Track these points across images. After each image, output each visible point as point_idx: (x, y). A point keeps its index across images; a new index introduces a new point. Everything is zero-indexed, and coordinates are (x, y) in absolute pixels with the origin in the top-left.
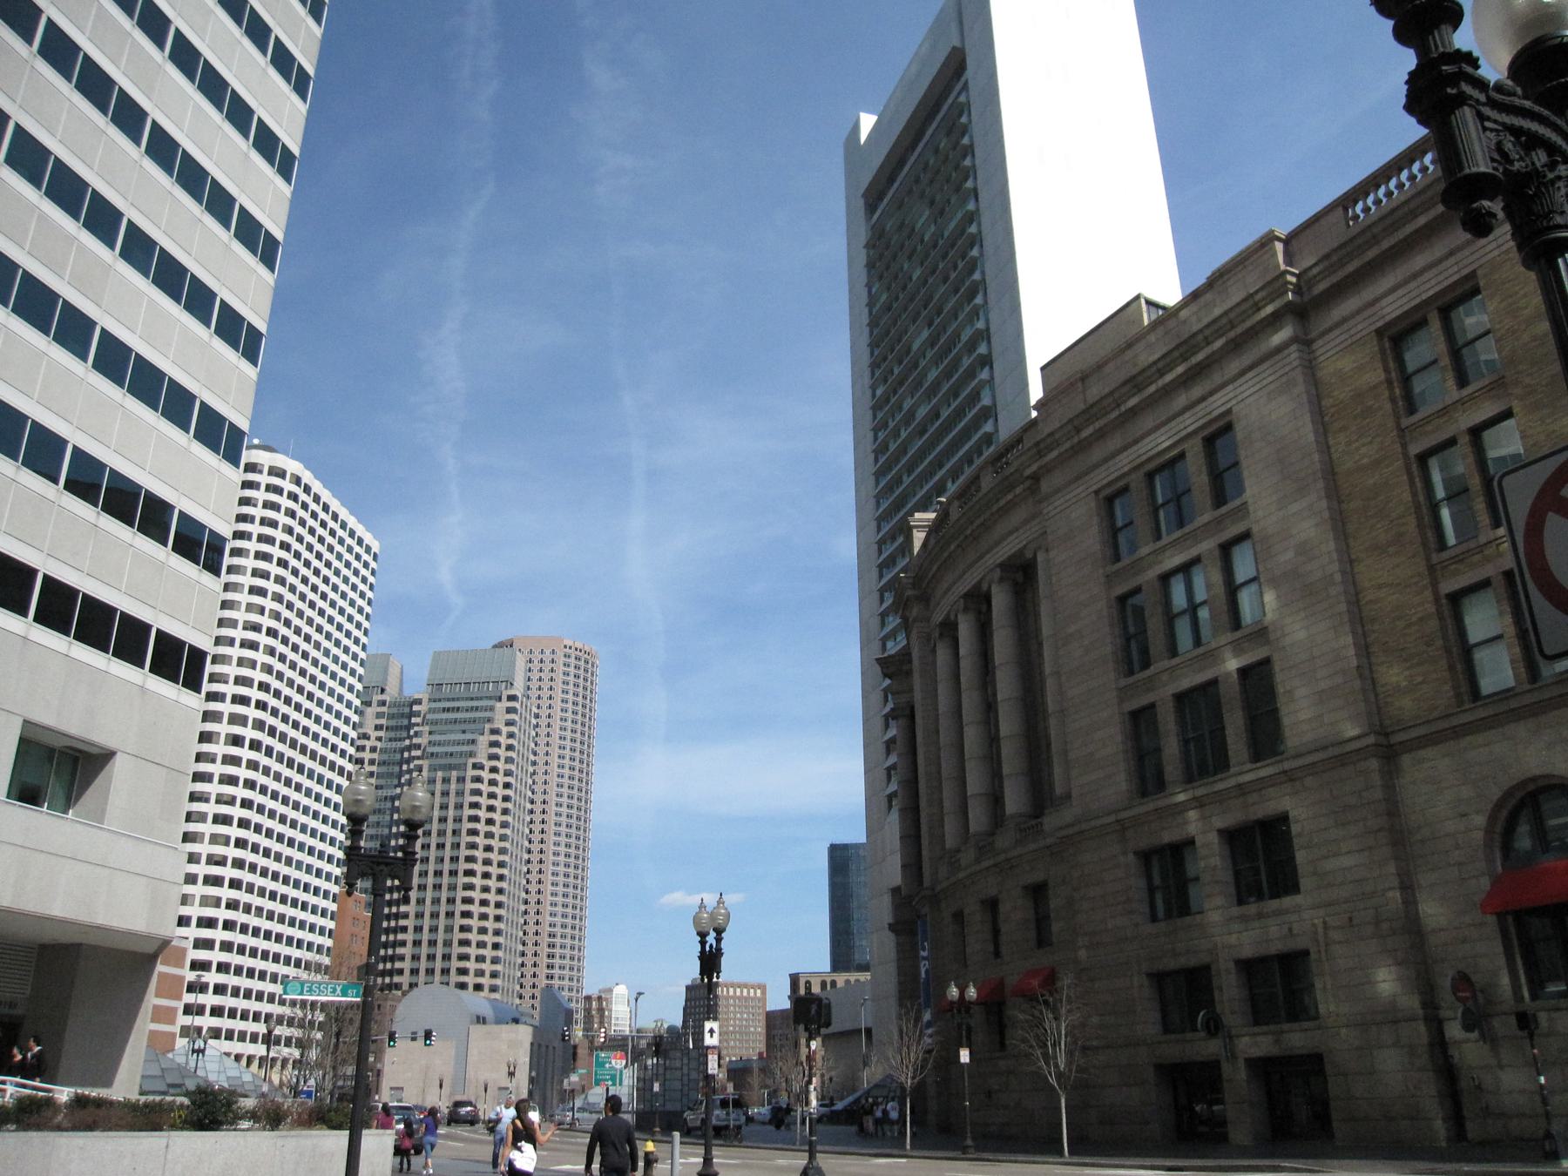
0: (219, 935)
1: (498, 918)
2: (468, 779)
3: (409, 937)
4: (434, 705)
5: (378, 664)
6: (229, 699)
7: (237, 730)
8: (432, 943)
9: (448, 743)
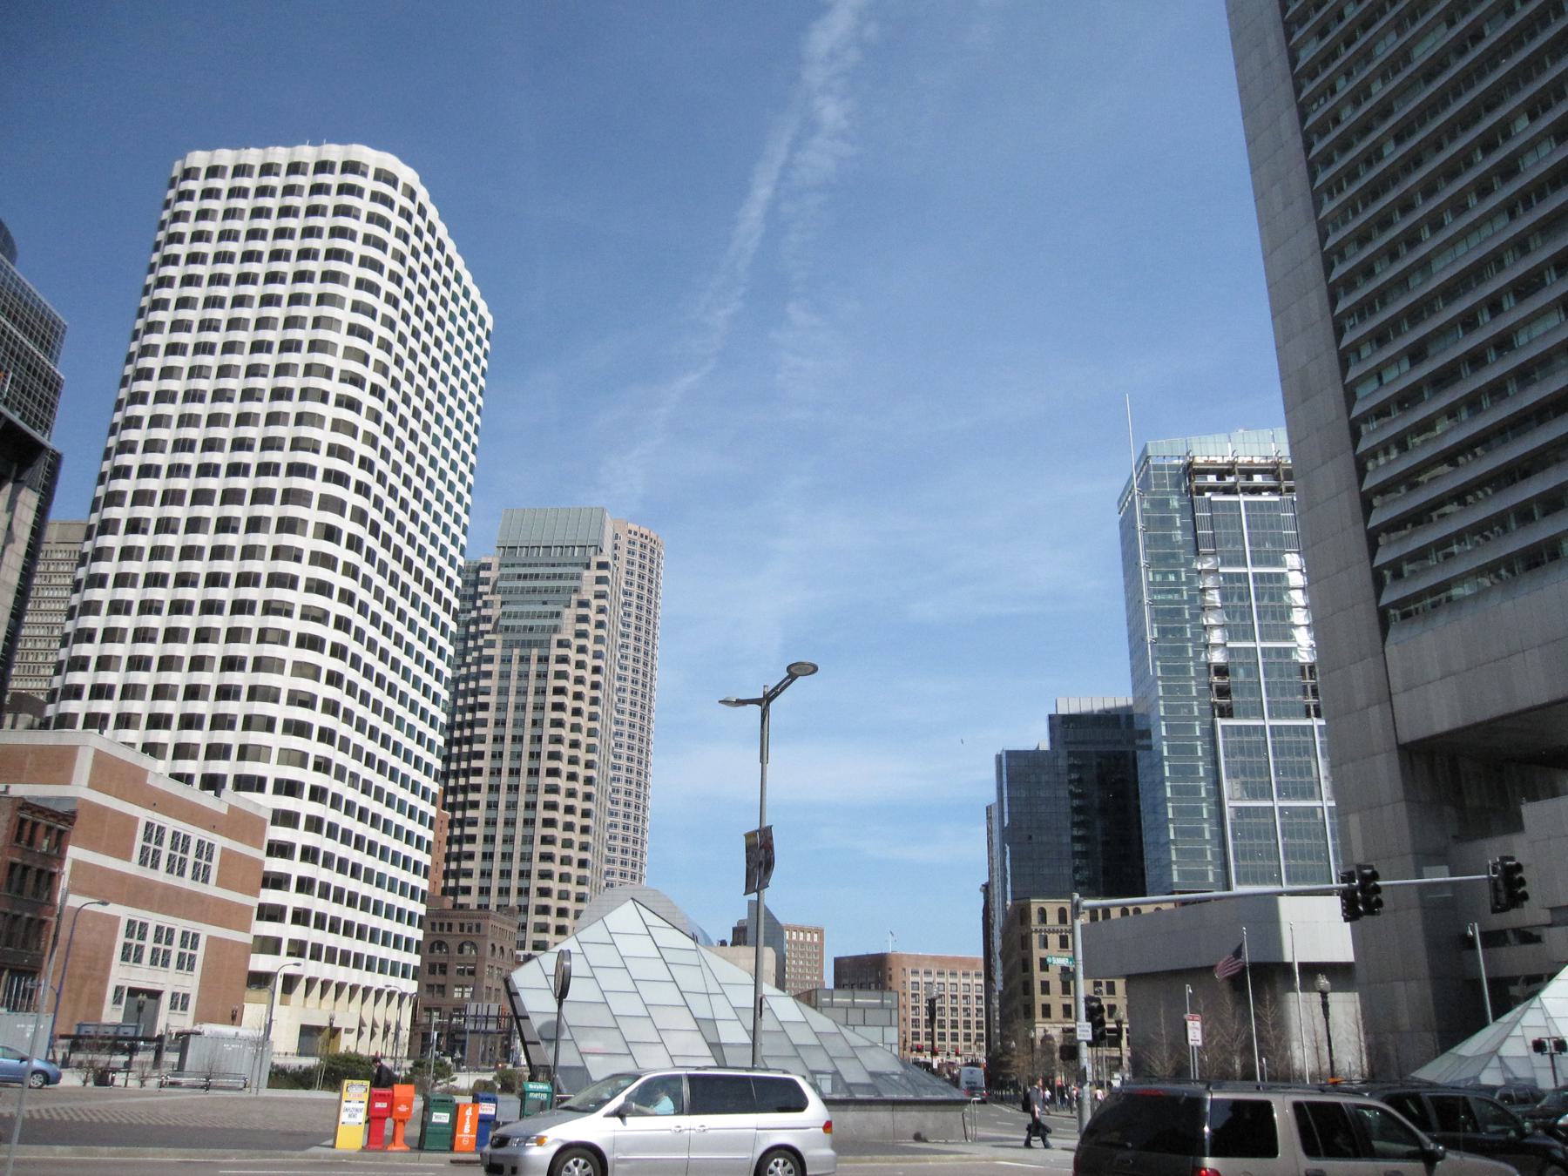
0: (304, 806)
1: (585, 830)
2: (552, 659)
3: (478, 848)
4: (505, 571)
6: (320, 474)
7: (331, 518)
8: (507, 857)
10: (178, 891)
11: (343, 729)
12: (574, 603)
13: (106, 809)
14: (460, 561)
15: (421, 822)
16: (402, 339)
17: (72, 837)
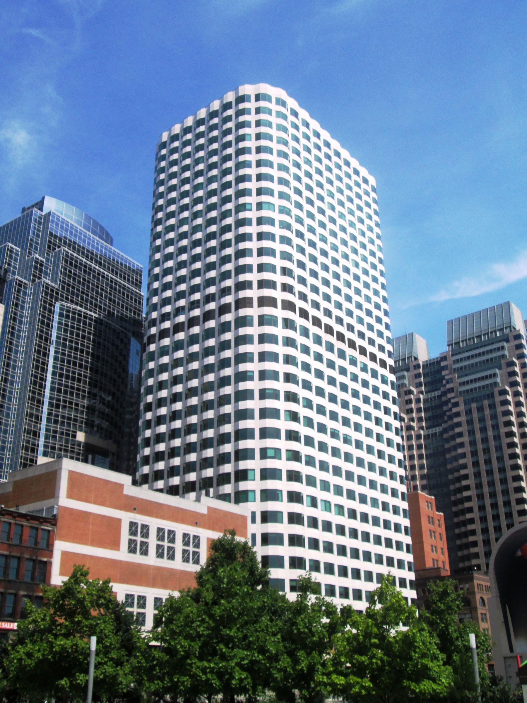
5: (407, 340)
13: (95, 503)
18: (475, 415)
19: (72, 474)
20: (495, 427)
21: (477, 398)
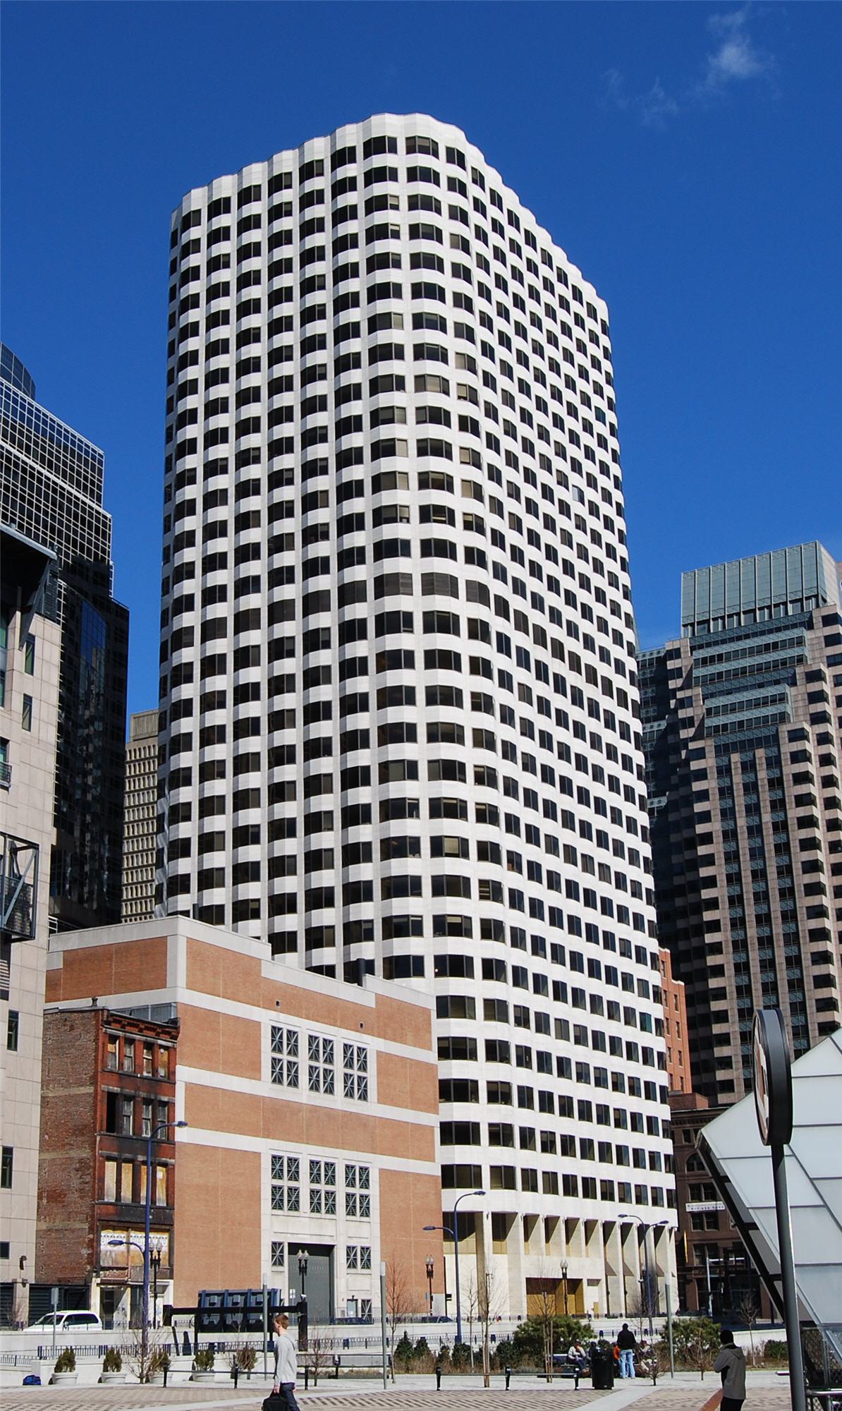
6: (416, 549)
9: (740, 707)
10: (330, 1114)
11: (513, 957)
12: (800, 678)
14: (631, 664)
15: (647, 1061)
16: (491, 412)
17: (178, 1060)
18: (738, 779)
19: (191, 942)
20: (778, 805)
21: (742, 742)
